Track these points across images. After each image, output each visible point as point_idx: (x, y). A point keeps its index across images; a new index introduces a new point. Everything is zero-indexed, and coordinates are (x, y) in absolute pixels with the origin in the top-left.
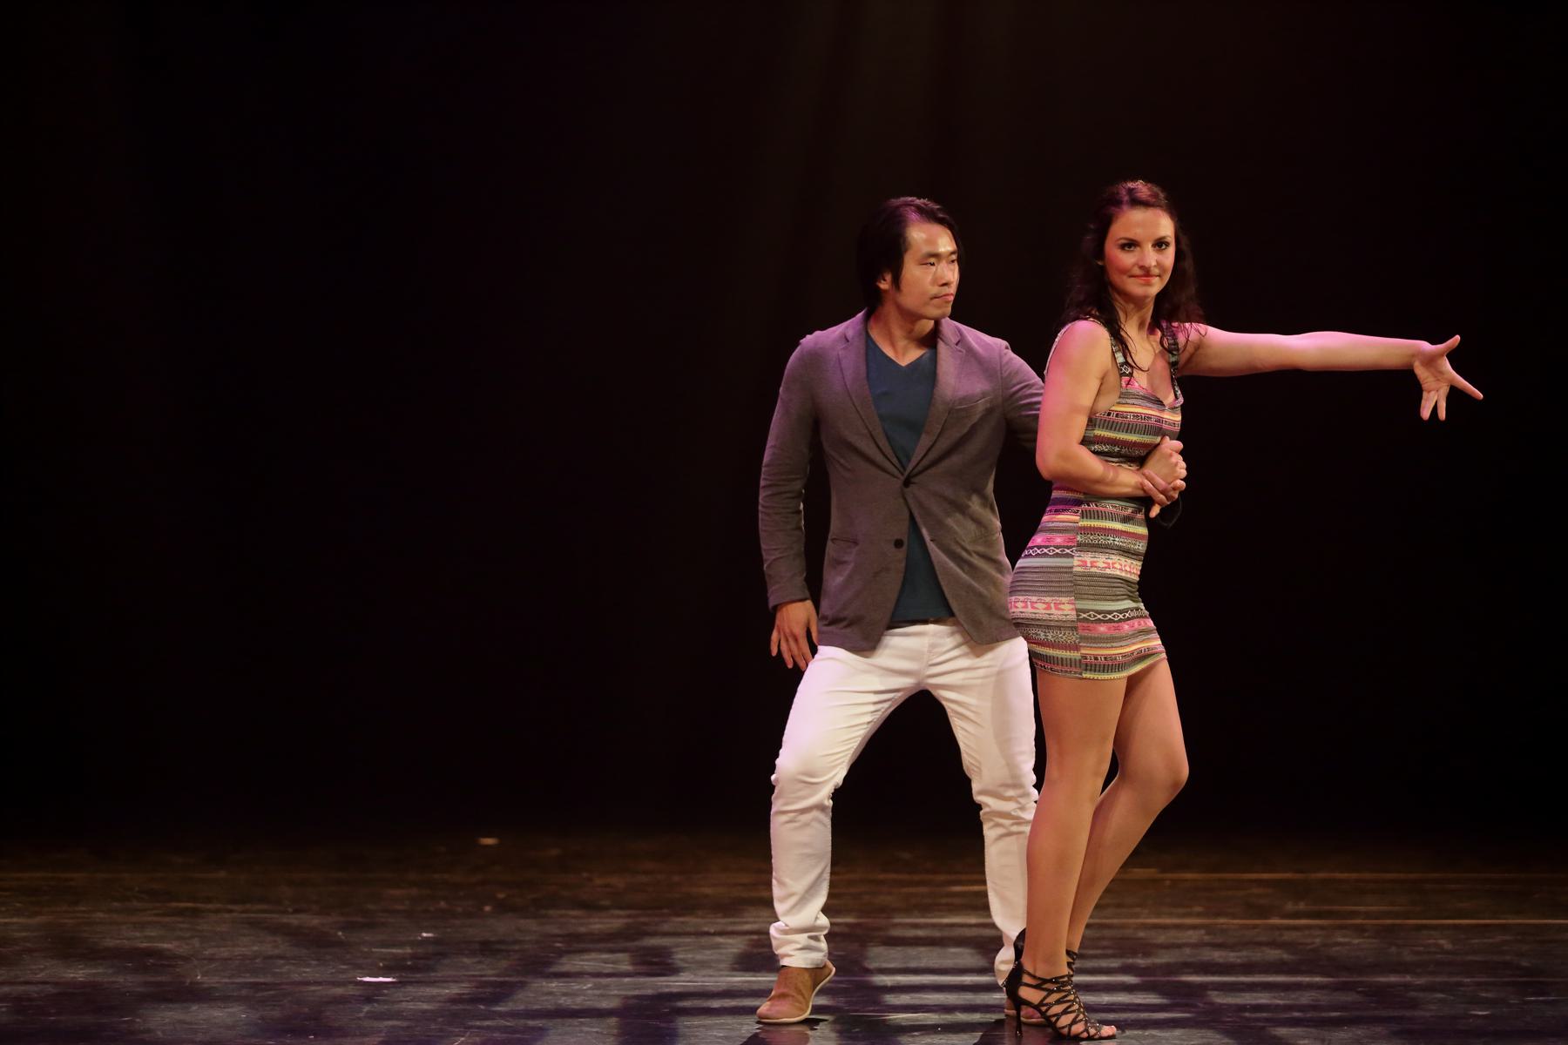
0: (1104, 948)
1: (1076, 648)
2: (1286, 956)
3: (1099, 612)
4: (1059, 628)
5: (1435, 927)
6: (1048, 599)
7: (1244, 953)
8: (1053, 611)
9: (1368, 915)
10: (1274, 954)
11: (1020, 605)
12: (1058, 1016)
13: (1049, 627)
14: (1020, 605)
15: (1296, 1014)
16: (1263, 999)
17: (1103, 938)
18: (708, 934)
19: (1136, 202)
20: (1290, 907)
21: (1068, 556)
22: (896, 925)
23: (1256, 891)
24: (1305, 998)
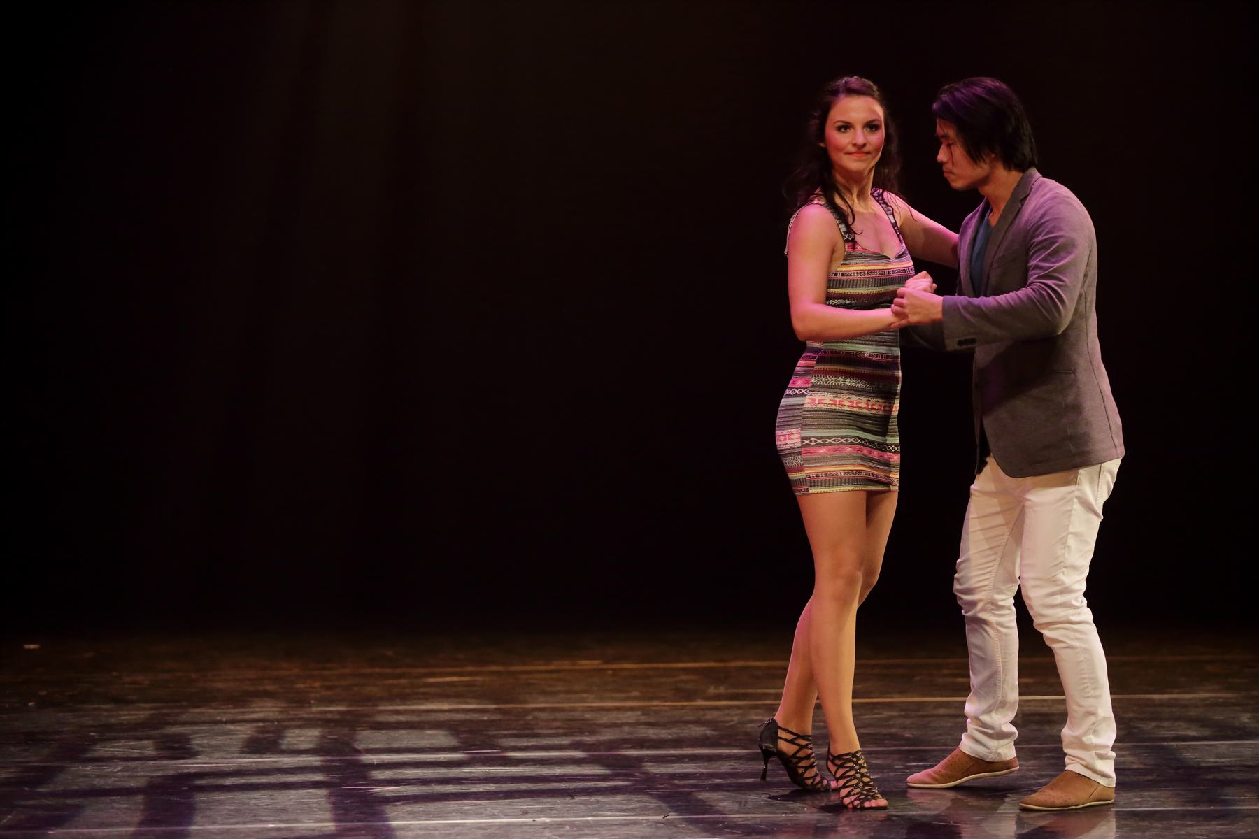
2: (708, 732)
7: (674, 730)
10: (698, 731)
15: (718, 781)
16: (690, 768)
17: (555, 720)
18: (221, 722)
19: (851, 91)
20: (712, 690)
24: (725, 767)
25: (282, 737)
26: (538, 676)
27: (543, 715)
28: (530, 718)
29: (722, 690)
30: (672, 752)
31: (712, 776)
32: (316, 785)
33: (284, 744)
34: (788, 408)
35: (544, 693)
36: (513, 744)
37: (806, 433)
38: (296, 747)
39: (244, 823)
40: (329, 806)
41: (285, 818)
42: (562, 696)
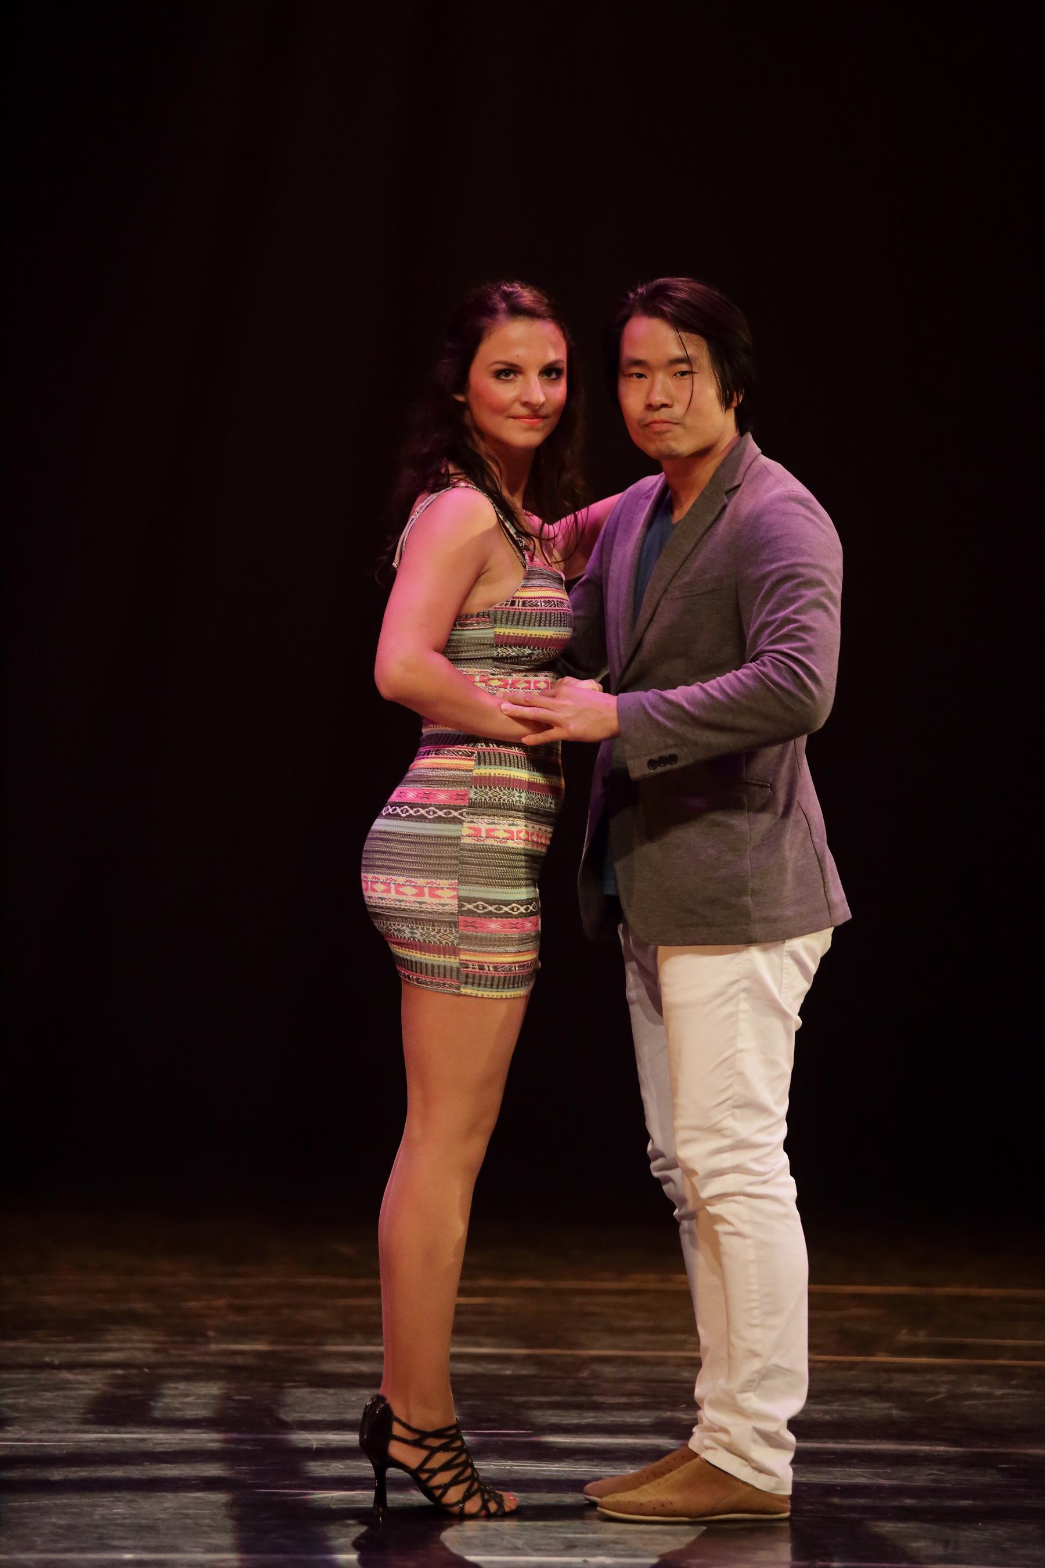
1: (454, 951)
3: (491, 903)
4: (432, 922)
6: (420, 882)
7: (835, 1406)
8: (427, 898)
9: (1017, 1353)
10: (876, 1409)
11: (380, 887)
12: (446, 1487)
13: (417, 921)
14: (380, 887)
15: (909, 1502)
16: (860, 1476)
18: (51, 1366)
19: (517, 311)
20: (904, 1337)
21: (455, 821)
22: (329, 1355)
24: (922, 1477)
26: (603, 1299)
27: (608, 1370)
28: (585, 1374)
29: (921, 1337)
32: (210, 1484)
33: (159, 1408)
35: (611, 1330)
36: (554, 1420)
37: (467, 891)
39: (82, 1550)
40: (229, 1523)
41: (153, 1542)
42: (642, 1337)
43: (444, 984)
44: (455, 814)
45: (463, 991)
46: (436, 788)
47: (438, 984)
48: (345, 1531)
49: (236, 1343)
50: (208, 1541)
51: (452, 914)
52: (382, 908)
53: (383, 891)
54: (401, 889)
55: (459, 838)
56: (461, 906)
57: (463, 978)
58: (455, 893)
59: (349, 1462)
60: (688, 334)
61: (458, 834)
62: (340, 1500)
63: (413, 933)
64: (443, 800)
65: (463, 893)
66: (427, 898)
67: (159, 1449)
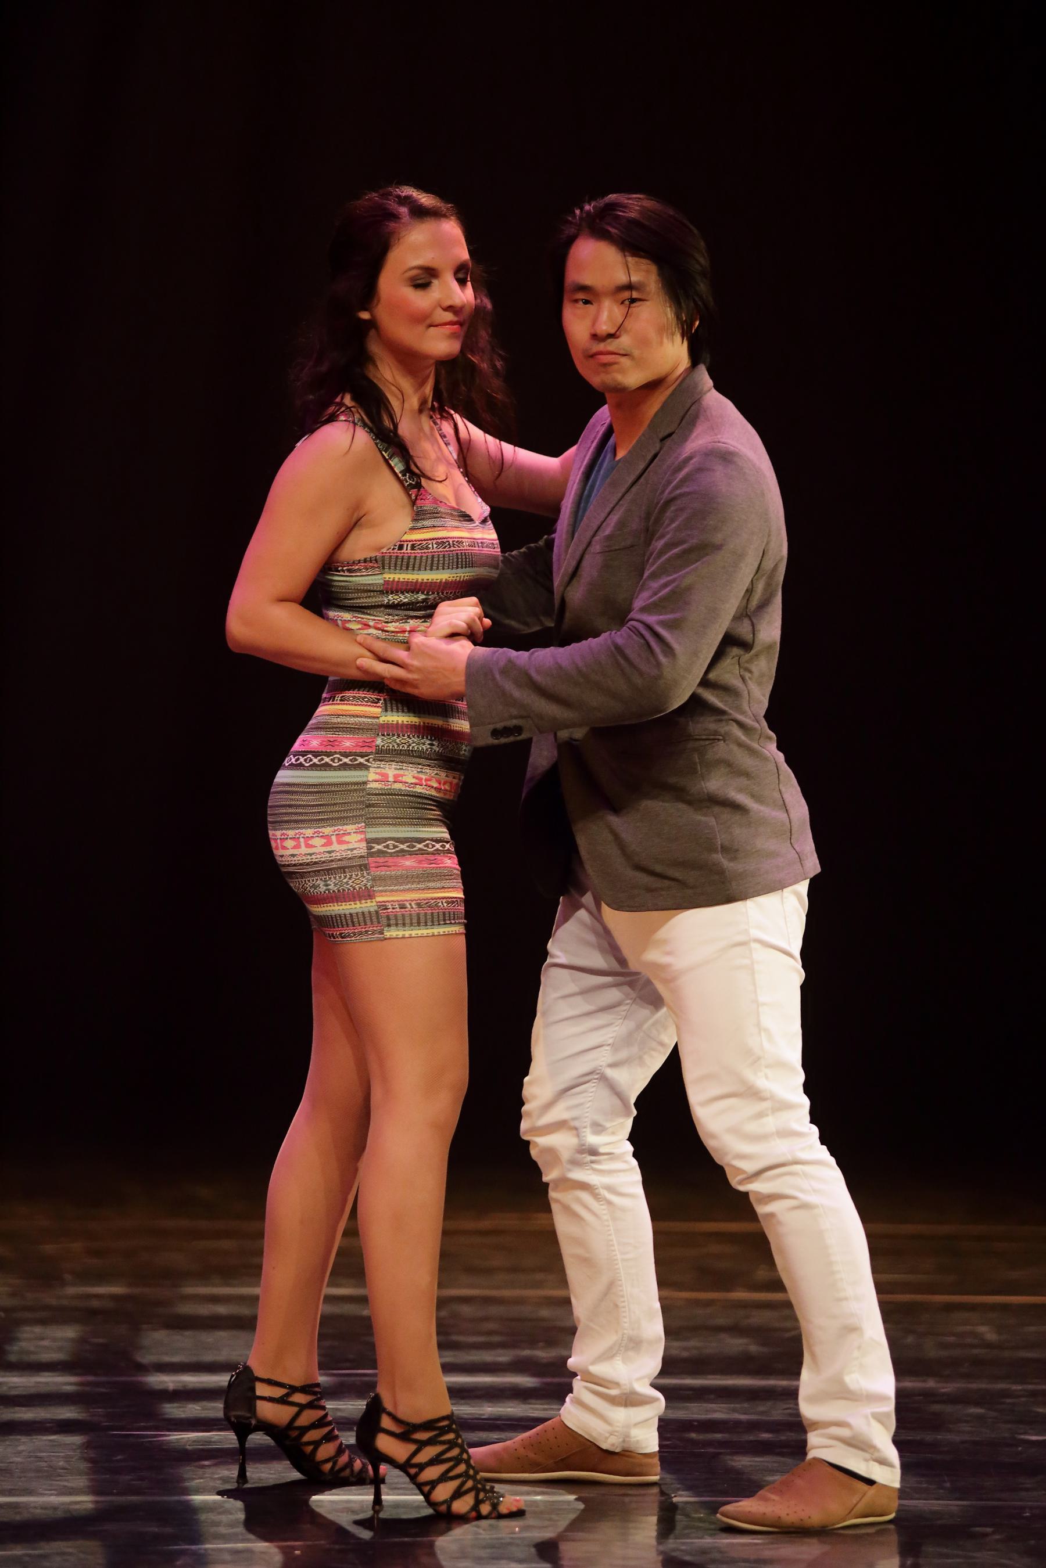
0: (490, 1333)
1: (370, 895)
2: (754, 1349)
4: (343, 869)
5: (973, 1307)
6: (327, 831)
7: (693, 1343)
8: (335, 846)
10: (736, 1345)
11: (289, 844)
12: (317, 1444)
14: (289, 844)
15: (766, 1436)
16: (718, 1411)
17: (486, 1319)
19: (420, 213)
21: (361, 767)
23: (715, 1248)
25: (12, 1340)
27: (466, 1310)
30: (689, 1381)
31: (753, 1426)
33: (15, 1352)
34: (291, 789)
35: (471, 1270)
37: (374, 833)
38: (33, 1358)
40: (84, 1466)
43: (366, 932)
44: (361, 760)
45: (387, 934)
46: (342, 735)
47: (361, 933)
48: (200, 1472)
49: (93, 1285)
50: (62, 1483)
51: (361, 857)
52: (295, 865)
53: (295, 847)
54: (310, 842)
55: (365, 783)
56: (369, 848)
57: (384, 921)
58: (363, 836)
59: (205, 1404)
60: (637, 259)
61: (364, 779)
62: (196, 1441)
63: (327, 885)
64: (348, 748)
65: (370, 836)
66: (335, 846)
67: (14, 1392)
